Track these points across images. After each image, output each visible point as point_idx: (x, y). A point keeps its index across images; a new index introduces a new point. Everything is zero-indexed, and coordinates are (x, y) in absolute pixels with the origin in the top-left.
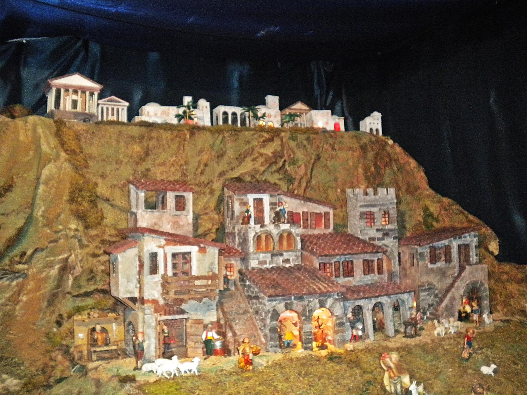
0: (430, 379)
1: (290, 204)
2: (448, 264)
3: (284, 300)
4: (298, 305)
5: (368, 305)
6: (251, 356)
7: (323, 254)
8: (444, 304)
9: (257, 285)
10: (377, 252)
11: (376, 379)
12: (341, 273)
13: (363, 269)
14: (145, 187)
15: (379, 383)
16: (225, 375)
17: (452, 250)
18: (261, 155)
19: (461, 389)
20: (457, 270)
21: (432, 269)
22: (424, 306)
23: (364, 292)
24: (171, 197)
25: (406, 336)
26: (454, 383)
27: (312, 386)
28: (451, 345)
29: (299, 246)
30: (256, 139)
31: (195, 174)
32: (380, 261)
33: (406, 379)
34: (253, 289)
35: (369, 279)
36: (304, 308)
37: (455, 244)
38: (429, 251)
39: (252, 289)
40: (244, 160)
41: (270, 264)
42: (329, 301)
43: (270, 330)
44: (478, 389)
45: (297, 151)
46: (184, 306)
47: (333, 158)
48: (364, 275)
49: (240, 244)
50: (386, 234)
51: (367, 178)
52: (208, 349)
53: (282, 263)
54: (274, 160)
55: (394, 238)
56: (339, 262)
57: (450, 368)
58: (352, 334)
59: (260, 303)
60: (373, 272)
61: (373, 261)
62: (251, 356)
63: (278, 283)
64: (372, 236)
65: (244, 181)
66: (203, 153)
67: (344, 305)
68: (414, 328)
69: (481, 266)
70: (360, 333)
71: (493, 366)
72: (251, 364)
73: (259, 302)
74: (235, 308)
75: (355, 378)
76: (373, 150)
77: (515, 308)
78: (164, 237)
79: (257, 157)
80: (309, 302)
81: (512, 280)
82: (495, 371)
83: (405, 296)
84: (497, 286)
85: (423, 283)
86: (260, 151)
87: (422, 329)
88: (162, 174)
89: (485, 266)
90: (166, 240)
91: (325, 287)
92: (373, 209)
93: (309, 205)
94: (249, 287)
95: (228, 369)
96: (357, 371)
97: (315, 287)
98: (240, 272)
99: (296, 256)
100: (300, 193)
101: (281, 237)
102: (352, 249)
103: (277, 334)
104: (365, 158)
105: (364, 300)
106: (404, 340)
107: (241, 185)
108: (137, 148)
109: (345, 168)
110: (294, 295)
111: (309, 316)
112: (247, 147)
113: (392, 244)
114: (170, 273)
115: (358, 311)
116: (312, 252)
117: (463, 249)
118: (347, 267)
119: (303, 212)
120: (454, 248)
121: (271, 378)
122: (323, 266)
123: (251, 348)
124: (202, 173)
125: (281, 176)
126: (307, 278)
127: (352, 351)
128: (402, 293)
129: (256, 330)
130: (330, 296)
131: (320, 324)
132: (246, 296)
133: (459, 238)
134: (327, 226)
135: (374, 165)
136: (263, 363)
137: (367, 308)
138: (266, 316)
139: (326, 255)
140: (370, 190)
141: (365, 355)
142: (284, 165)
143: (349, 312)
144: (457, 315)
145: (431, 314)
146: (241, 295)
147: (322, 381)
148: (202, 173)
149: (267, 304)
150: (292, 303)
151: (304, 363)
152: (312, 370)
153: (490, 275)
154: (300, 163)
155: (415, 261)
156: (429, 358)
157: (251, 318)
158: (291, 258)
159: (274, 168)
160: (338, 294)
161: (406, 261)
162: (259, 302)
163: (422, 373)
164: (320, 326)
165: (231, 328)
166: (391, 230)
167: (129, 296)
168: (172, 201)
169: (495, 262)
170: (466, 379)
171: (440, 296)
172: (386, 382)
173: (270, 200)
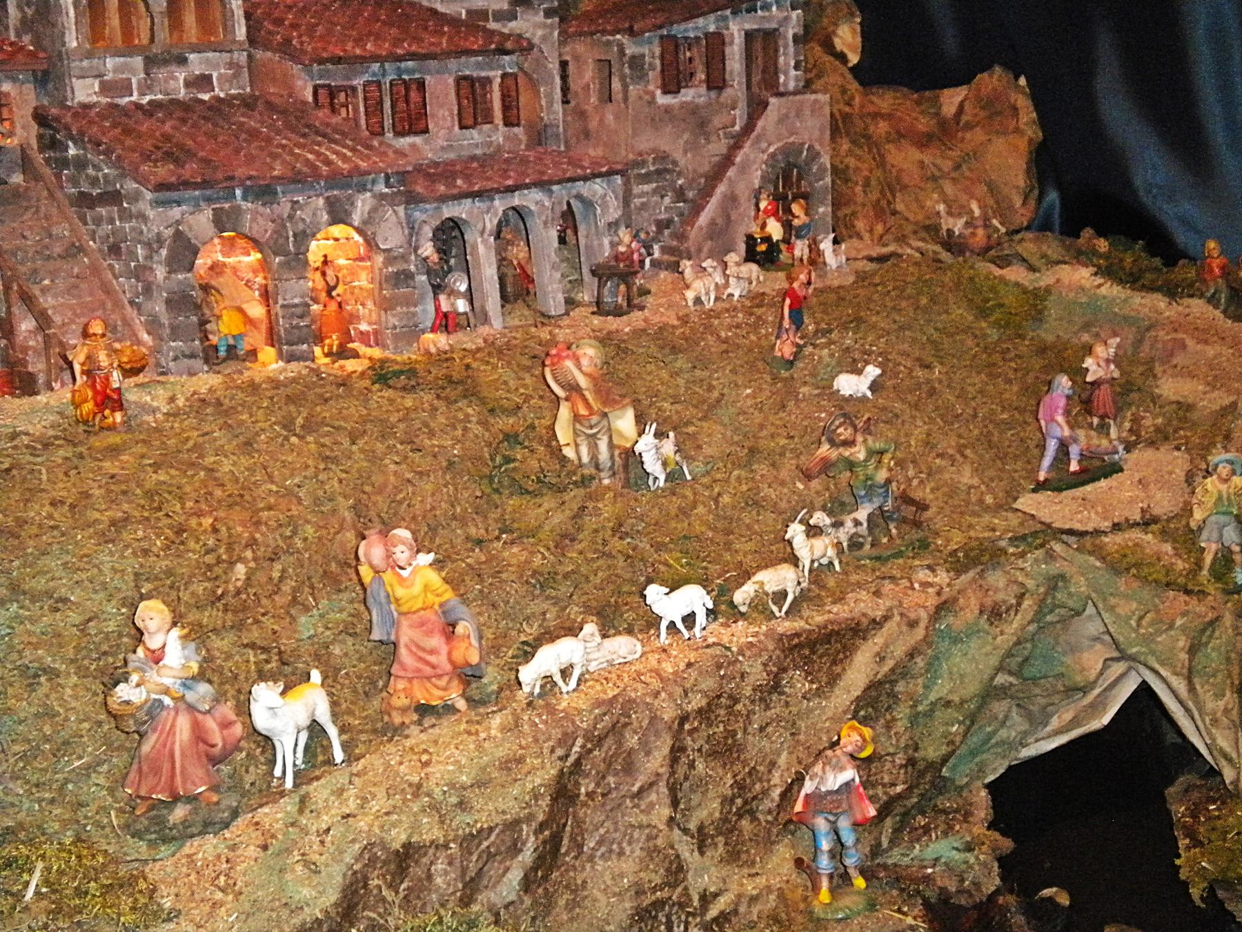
0: (688, 423)
2: (713, 94)
3: (209, 200)
4: (256, 217)
5: (480, 218)
6: (116, 378)
7: (325, 55)
8: (703, 219)
9: (107, 153)
11: (532, 427)
12: (388, 122)
13: (456, 108)
15: (541, 441)
16: (27, 447)
17: (728, 50)
19: (783, 442)
20: (740, 115)
21: (668, 110)
23: (467, 178)
25: (600, 308)
26: (762, 427)
27: (335, 461)
28: (738, 326)
29: (241, 32)
33: (625, 422)
34: (97, 168)
36: (280, 224)
37: (736, 29)
38: (657, 51)
39: (90, 171)
41: (142, 94)
43: (168, 302)
44: (841, 430)
48: (462, 127)
49: (26, 25)
53: (183, 91)
56: (379, 84)
57: (746, 387)
58: (438, 308)
59: (126, 216)
60: (489, 120)
61: (489, 80)
62: (116, 378)
63: (181, 147)
67: (408, 216)
68: (623, 288)
69: (813, 97)
70: (462, 305)
71: (872, 371)
72: (119, 405)
73: (122, 211)
74: (33, 238)
75: (465, 429)
77: (907, 219)
81: (900, 135)
82: (874, 386)
83: (597, 188)
84: (859, 159)
85: (640, 154)
87: (645, 292)
89: (824, 98)
91: (344, 158)
94: (81, 164)
95: (36, 428)
96: (470, 411)
97: (310, 156)
98: (40, 117)
99: (231, 65)
102: (417, 40)
103: (194, 306)
105: (470, 200)
106: (596, 321)
110: (242, 184)
113: (540, 33)
115: (450, 235)
116: (285, 48)
117: (758, 45)
118: (407, 96)
120: (732, 43)
121: (191, 443)
122: (330, 96)
123: (113, 352)
126: (278, 132)
128: (585, 179)
129: (117, 304)
130: (362, 188)
131: (332, 284)
132: (68, 197)
133: (748, 11)
136: (155, 404)
137: (480, 226)
138: (149, 257)
139: (338, 60)
141: (488, 363)
143: (422, 241)
144: (742, 247)
145: (664, 250)
146: (51, 195)
147: (361, 443)
149: (151, 214)
151: (291, 394)
153: (839, 126)
155: (616, 85)
156: (681, 362)
157: (95, 270)
160: (387, 177)
162: (122, 211)
164: (330, 290)
165: (28, 300)
169: (854, 86)
170: (793, 414)
171: (690, 195)
172: (563, 433)
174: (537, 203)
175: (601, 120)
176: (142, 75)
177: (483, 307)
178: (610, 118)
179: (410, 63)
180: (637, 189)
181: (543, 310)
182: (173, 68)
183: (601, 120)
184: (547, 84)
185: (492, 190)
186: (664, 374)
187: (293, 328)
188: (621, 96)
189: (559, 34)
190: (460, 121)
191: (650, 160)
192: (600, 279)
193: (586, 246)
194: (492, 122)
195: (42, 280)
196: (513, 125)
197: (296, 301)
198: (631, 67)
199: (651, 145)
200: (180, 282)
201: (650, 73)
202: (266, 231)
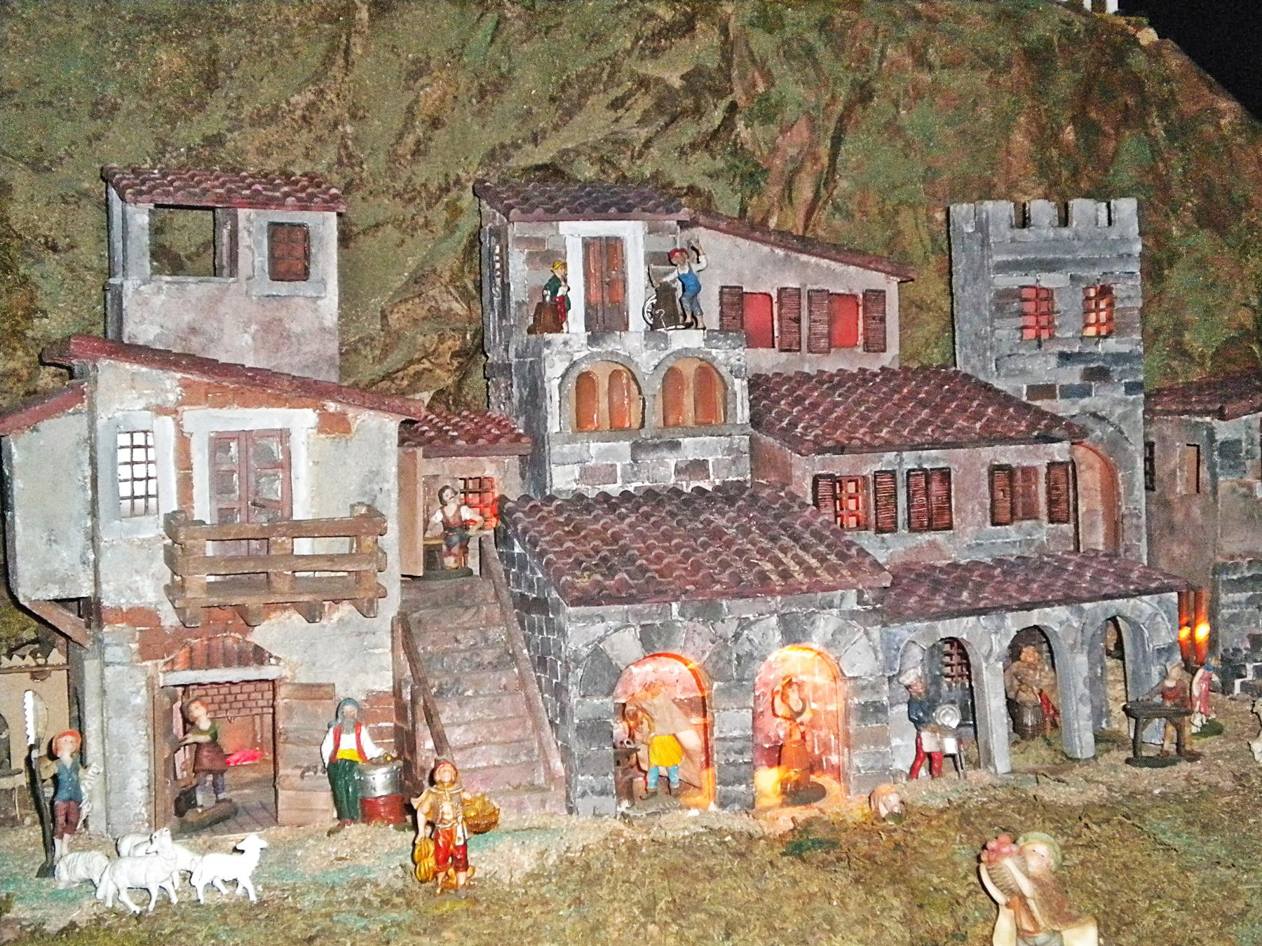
1: (725, 260)
5: (988, 638)
6: (460, 833)
7: (828, 444)
10: (1049, 439)
12: (902, 517)
13: (988, 502)
14: (150, 192)
18: (644, 83)
22: (1236, 643)
24: (252, 227)
29: (743, 414)
30: (627, 26)
31: (393, 158)
32: (1064, 473)
35: (1012, 538)
40: (580, 107)
42: (821, 623)
45: (778, 68)
46: (259, 636)
47: (919, 96)
51: (1045, 168)
52: (350, 802)
54: (688, 102)
55: (1132, 388)
56: (893, 474)
58: (919, 747)
60: (1031, 514)
62: (460, 833)
64: (1045, 380)
65: (570, 180)
66: (424, 80)
76: (1075, 66)
78: (179, 375)
79: (630, 94)
80: (744, 624)
83: (1146, 604)
85: (1232, 557)
86: (641, 71)
88: (264, 153)
90: (186, 386)
92: (1048, 280)
93: (805, 265)
99: (730, 450)
100: (788, 226)
101: (672, 377)
104: (1038, 95)
107: (556, 191)
108: (169, 58)
109: (964, 132)
111: (740, 680)
112: (590, 57)
113: (1119, 410)
114: (203, 509)
116: (787, 435)
119: (781, 291)
124: (418, 151)
125: (720, 164)
127: (898, 817)
132: (512, 595)
134: (875, 345)
135: (1073, 120)
137: (985, 649)
140: (1043, 210)
142: (728, 123)
148: (418, 151)
151: (686, 863)
152: (705, 890)
154: (790, 112)
155: (1205, 475)
158: (716, 456)
159: (688, 131)
160: (860, 593)
161: (1173, 474)
163: (1170, 912)
165: (430, 718)
166: (1119, 358)
167: (55, 593)
168: (258, 243)
173: (646, 245)
174: (1061, 623)
175: (1187, 515)
176: (629, 461)
177: (987, 742)
178: (1196, 512)
179: (934, 452)
180: (1224, 598)
181: (1067, 750)
182: (665, 453)
183: (1187, 515)
184: (1126, 468)
185: (1002, 607)
186: (1173, 867)
187: (729, 764)
188: (1209, 488)
189: (1145, 412)
190: (993, 514)
191: (1245, 563)
192: (1137, 720)
193: (1134, 672)
194: (1036, 518)
195: (465, 691)
196: (1059, 521)
197: (736, 733)
198: (1220, 455)
199: (1247, 546)
200: (596, 707)
201: (1248, 463)
202: (704, 652)
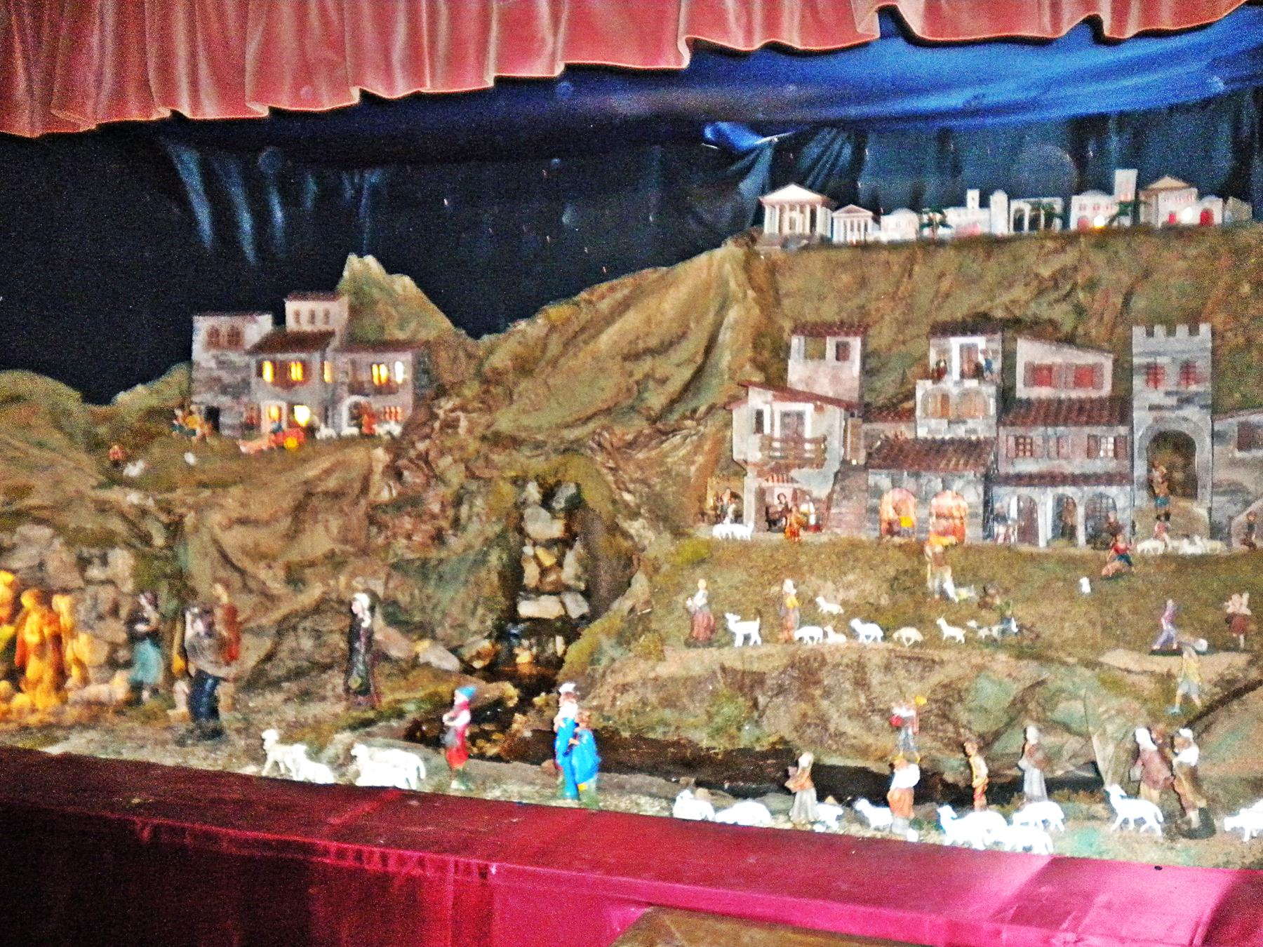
24: (830, 344)
50: (1185, 401)
108: (845, 278)
114: (777, 434)
142: (1073, 289)
150: (901, 479)
166: (1197, 394)
